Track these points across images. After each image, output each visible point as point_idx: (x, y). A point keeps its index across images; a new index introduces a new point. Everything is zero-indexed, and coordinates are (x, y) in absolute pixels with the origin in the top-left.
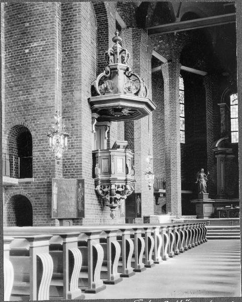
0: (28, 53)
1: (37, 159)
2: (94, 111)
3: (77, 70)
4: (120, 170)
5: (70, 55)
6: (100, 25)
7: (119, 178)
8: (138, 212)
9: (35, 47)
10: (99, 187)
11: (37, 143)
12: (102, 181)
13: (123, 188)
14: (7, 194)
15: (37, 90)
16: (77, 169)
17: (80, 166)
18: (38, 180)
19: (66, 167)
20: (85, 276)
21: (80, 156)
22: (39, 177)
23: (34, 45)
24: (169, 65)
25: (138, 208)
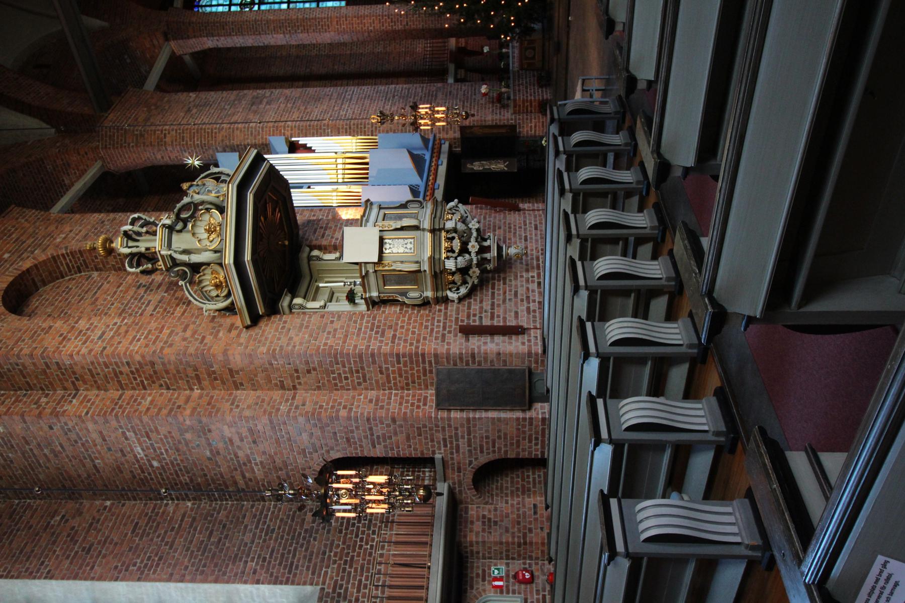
0: (160, 462)
1: (392, 449)
2: (273, 309)
3: (181, 363)
4: (409, 246)
5: (151, 376)
6: (87, 267)
7: (428, 253)
8: (504, 131)
9: (143, 450)
10: (451, 295)
11: (356, 449)
12: (436, 288)
13: (453, 238)
14: (473, 500)
15: (238, 447)
16: (412, 363)
17: (404, 356)
18: (440, 449)
19: (407, 384)
20: (611, 158)
21: (379, 357)
22: (433, 446)
23: (140, 451)
24: (175, 39)
25: (495, 131)
